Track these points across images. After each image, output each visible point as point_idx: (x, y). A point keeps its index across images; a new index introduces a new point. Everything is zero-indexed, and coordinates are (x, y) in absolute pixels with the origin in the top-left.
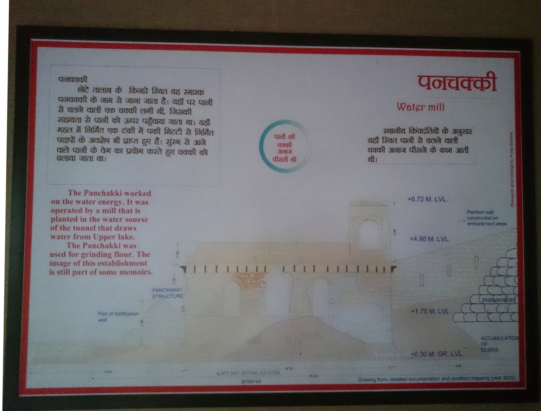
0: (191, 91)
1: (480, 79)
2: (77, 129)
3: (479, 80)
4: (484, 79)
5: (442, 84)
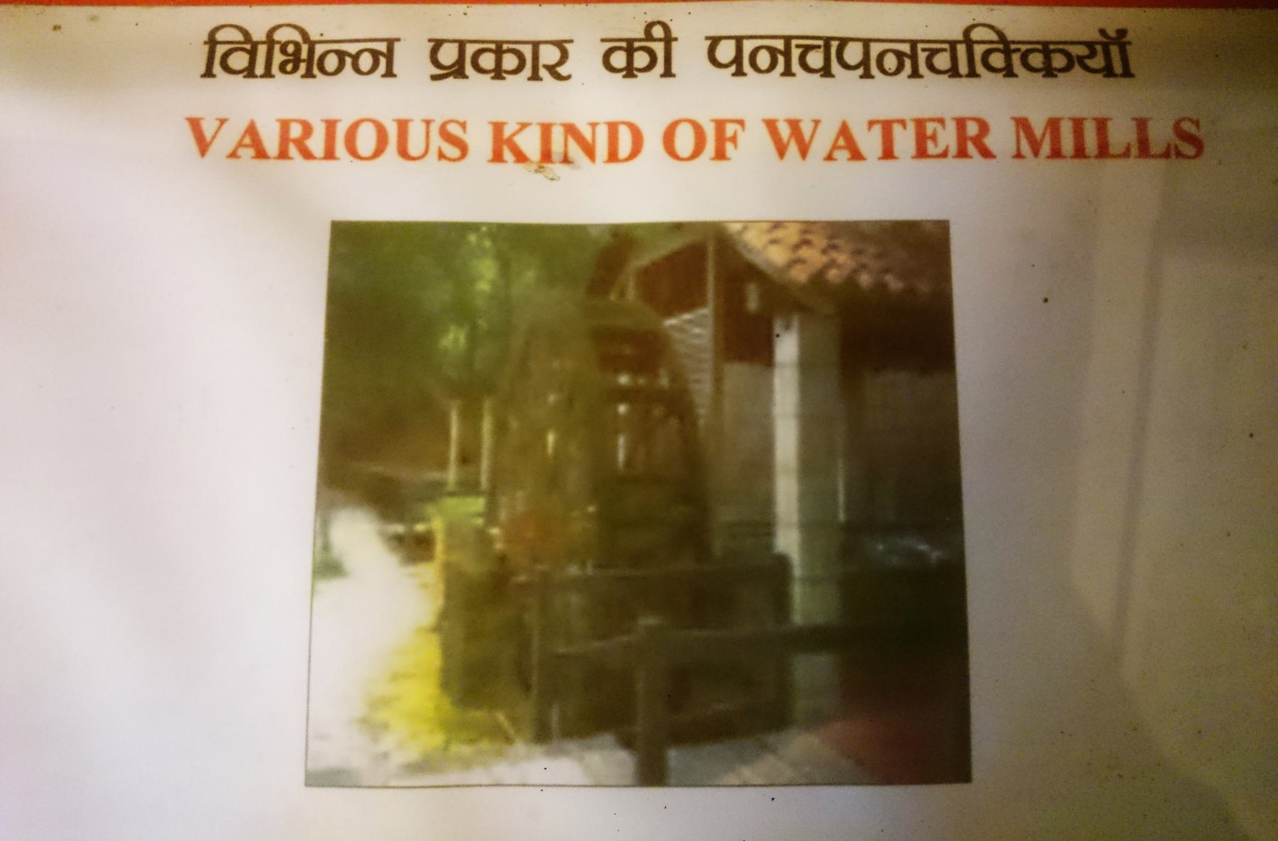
1: (821, 43)
3: (620, 48)
4: (637, 44)
5: (781, 59)
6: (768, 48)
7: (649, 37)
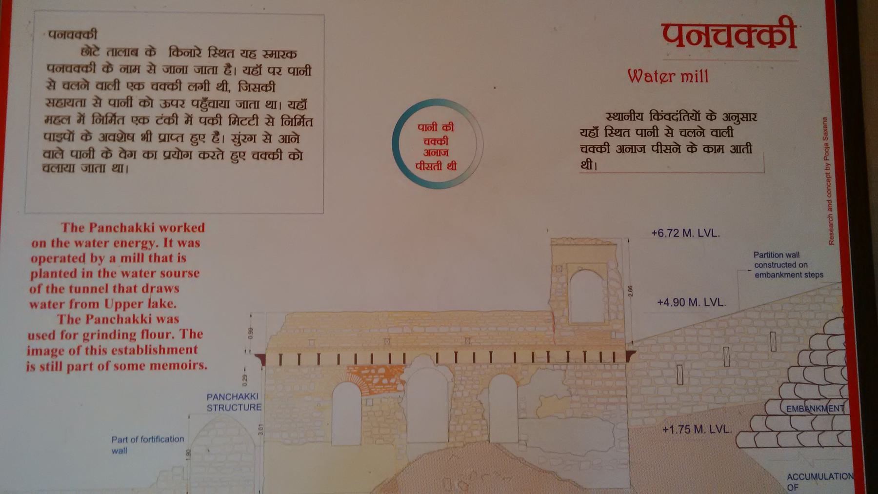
0: (274, 53)
2: (78, 118)
3: (744, 30)
4: (775, 29)
5: (704, 37)
6: (627, 115)
7: (781, 25)
